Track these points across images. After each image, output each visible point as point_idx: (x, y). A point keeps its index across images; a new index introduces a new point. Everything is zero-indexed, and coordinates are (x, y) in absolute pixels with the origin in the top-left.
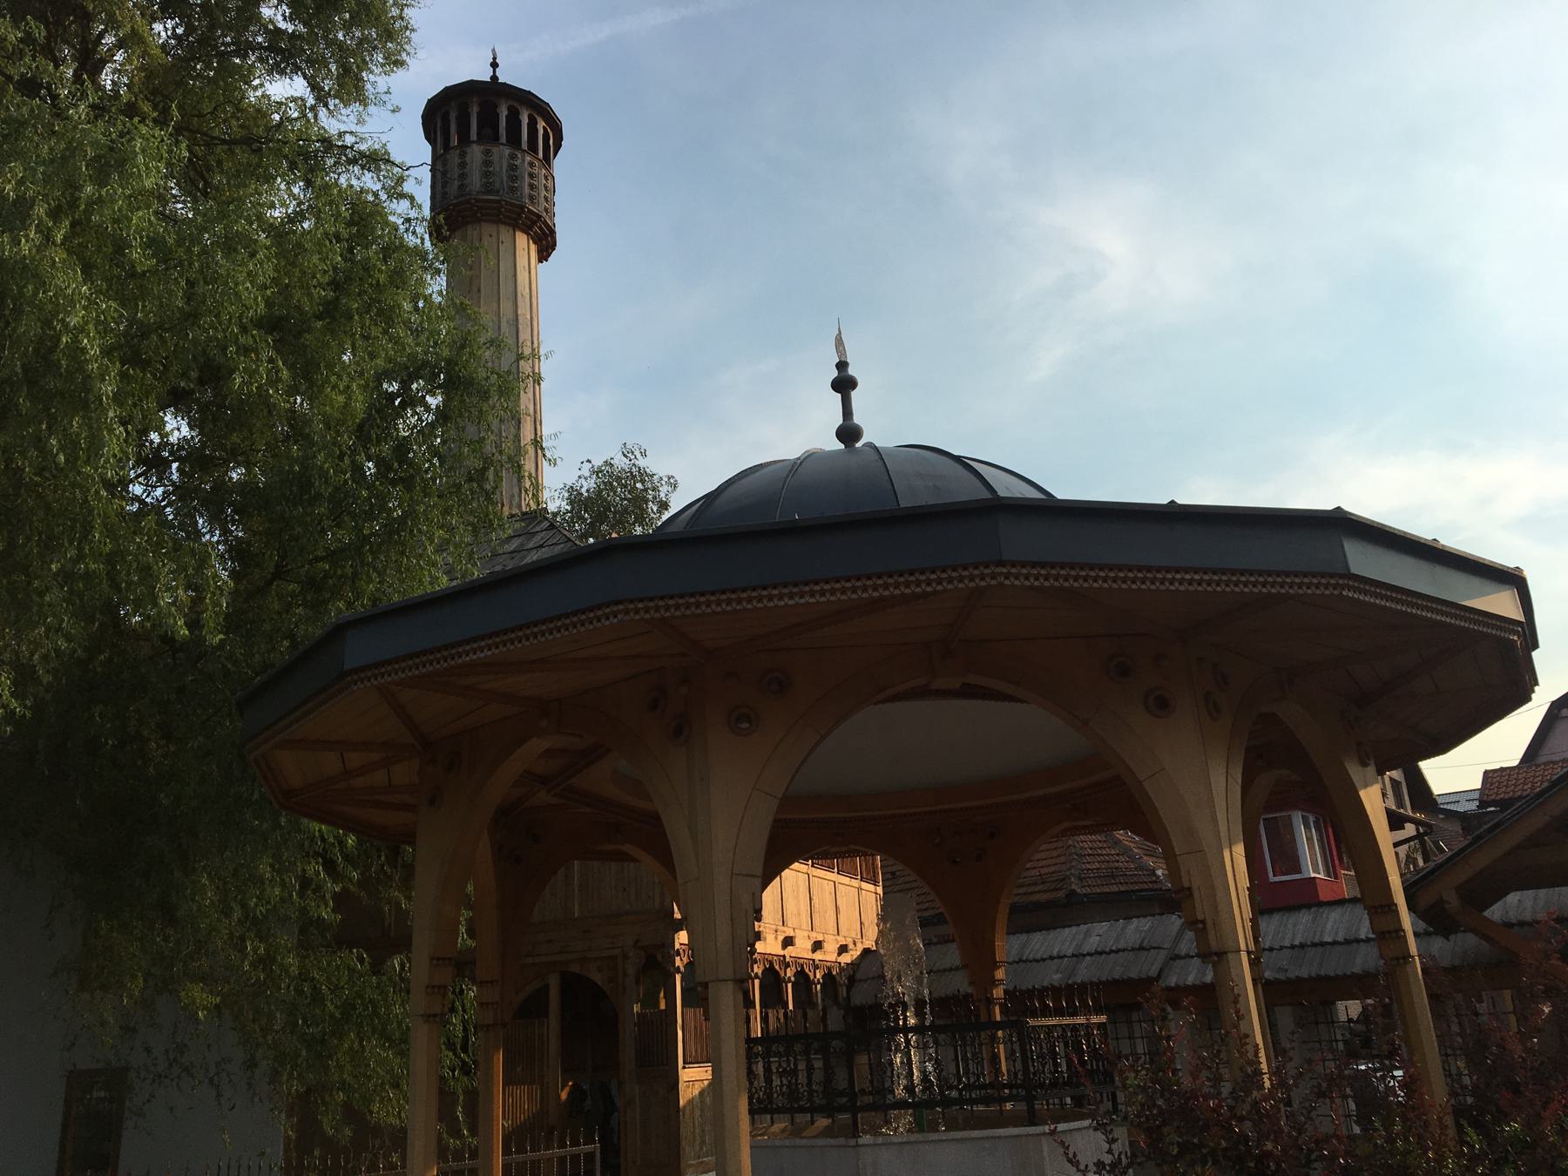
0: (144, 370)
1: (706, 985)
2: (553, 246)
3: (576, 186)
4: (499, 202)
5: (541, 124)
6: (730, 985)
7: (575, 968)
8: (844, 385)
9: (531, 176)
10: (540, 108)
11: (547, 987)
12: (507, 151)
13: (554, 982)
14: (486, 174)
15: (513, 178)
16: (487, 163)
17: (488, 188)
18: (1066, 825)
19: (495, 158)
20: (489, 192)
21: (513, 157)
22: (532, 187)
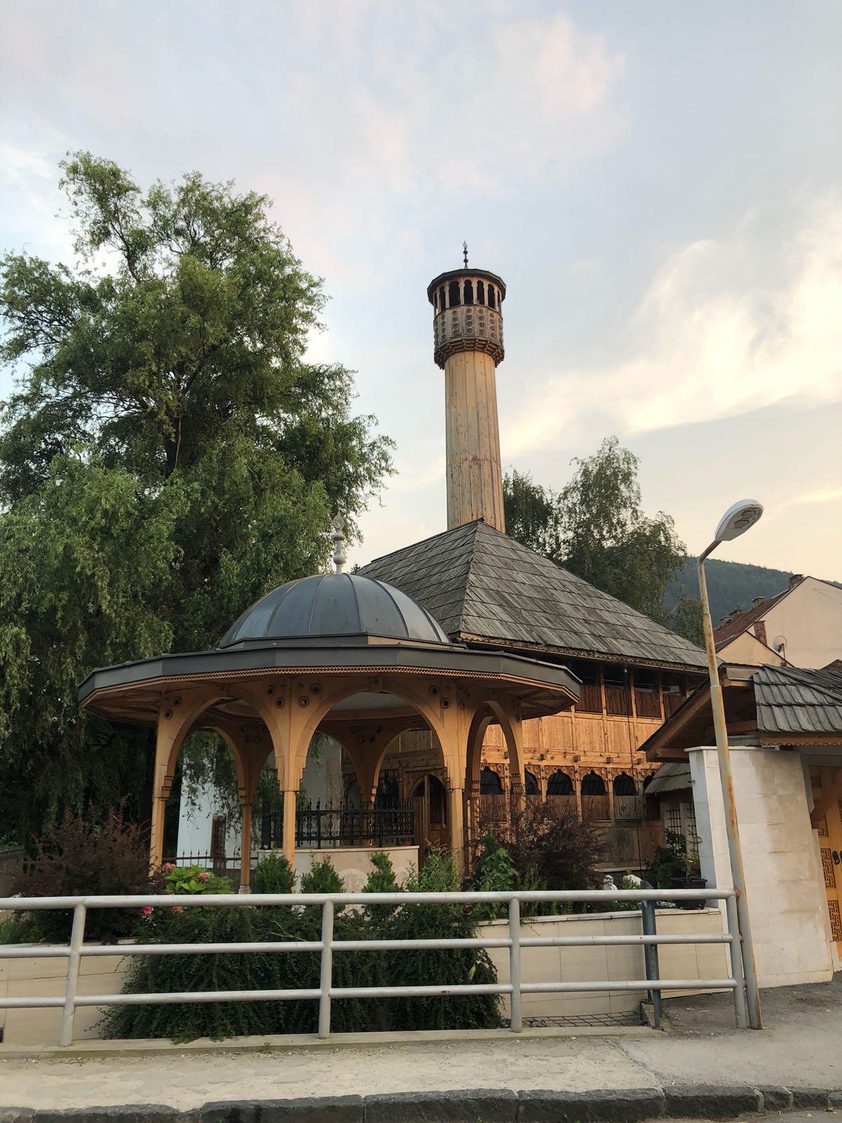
0: (309, 477)
1: (283, 792)
2: (502, 359)
3: (516, 320)
4: (461, 340)
5: (496, 289)
6: (293, 793)
7: (433, 774)
8: (466, 253)
9: (481, 318)
10: (496, 281)
11: (423, 783)
12: (465, 308)
13: (426, 779)
14: (455, 326)
15: (469, 324)
16: (455, 319)
17: (456, 334)
18: (565, 668)
19: (459, 315)
20: (455, 337)
21: (469, 311)
22: (492, 328)
